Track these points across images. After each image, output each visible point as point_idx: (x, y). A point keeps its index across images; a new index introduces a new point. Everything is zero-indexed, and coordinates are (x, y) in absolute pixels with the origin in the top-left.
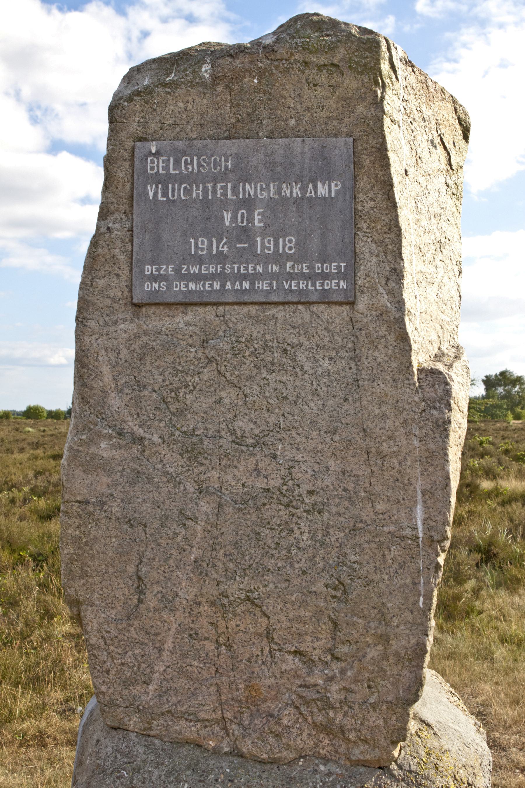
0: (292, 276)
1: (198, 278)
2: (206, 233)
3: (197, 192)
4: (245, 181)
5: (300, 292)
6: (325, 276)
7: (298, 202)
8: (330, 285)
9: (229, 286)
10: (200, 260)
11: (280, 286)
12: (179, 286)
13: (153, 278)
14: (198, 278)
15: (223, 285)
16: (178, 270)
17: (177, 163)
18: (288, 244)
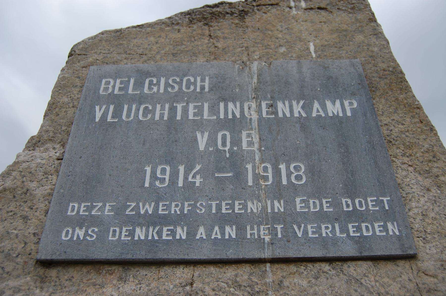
0: (306, 217)
1: (154, 220)
2: (170, 159)
3: (161, 112)
4: (225, 100)
5: (324, 242)
6: (357, 216)
7: (304, 124)
8: (373, 230)
9: (201, 232)
10: (157, 196)
11: (289, 236)
12: (118, 235)
13: (80, 222)
14: (154, 220)
15: (191, 234)
16: (119, 211)
17: (139, 84)
18: (294, 172)
